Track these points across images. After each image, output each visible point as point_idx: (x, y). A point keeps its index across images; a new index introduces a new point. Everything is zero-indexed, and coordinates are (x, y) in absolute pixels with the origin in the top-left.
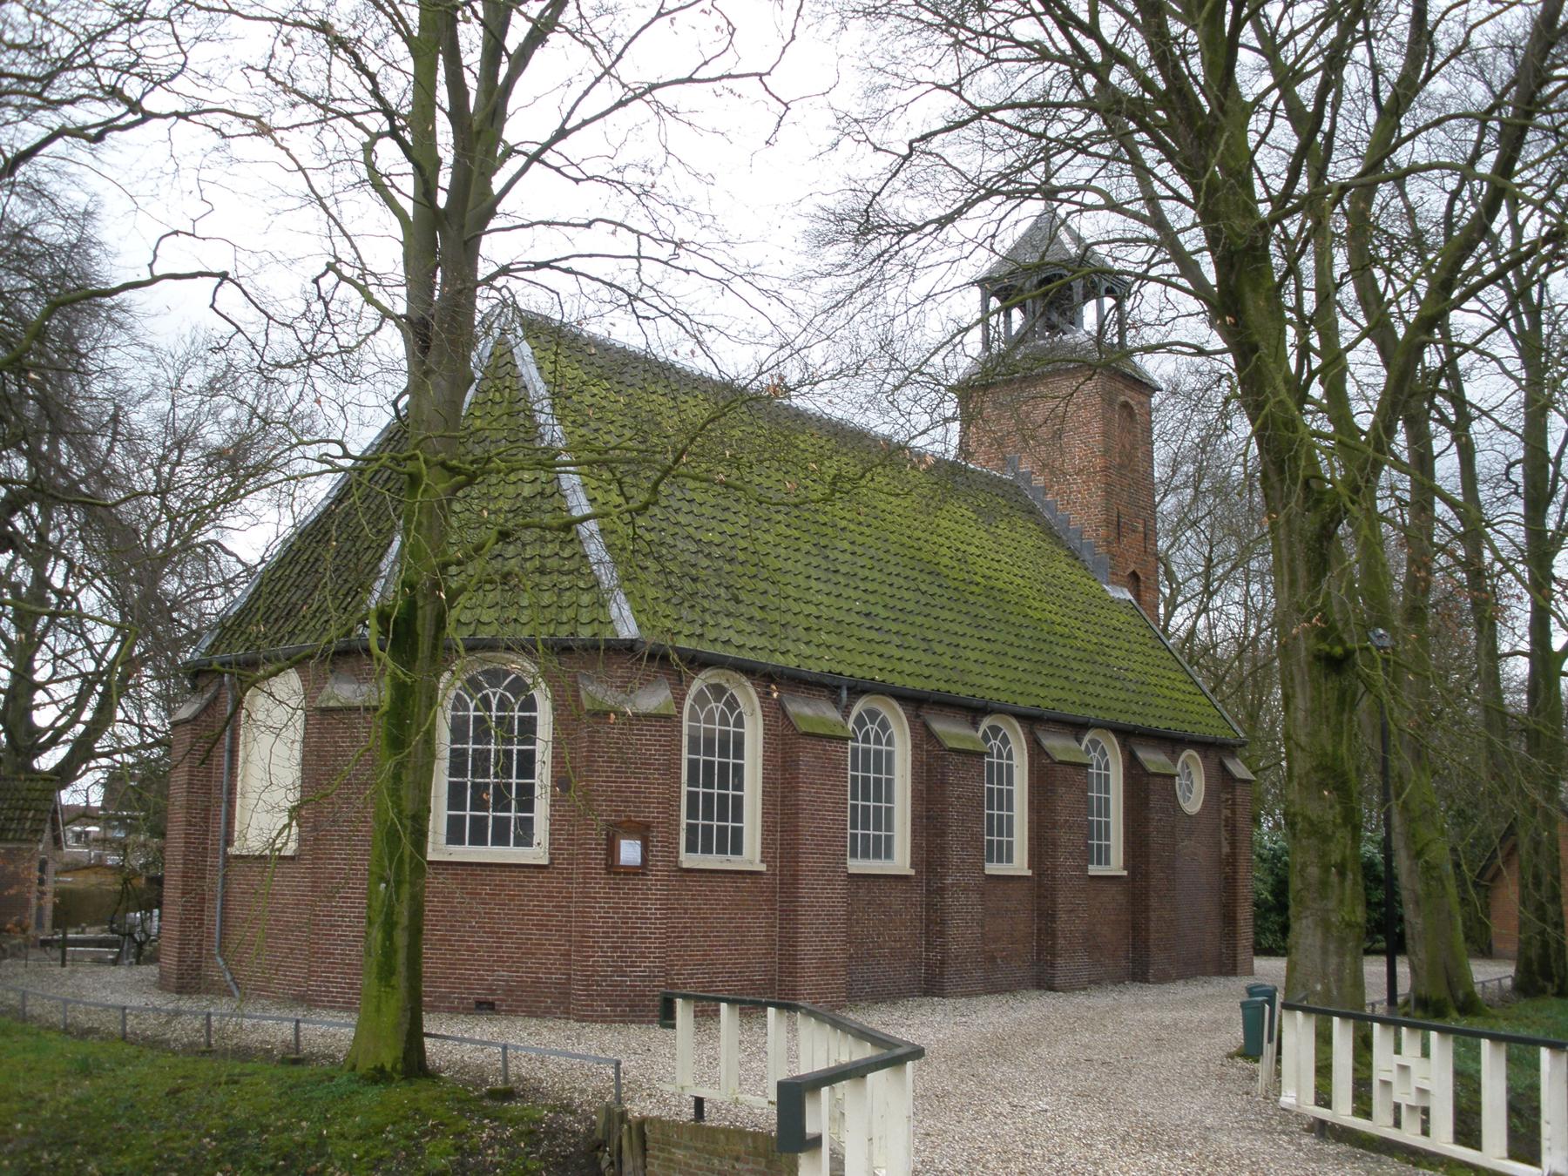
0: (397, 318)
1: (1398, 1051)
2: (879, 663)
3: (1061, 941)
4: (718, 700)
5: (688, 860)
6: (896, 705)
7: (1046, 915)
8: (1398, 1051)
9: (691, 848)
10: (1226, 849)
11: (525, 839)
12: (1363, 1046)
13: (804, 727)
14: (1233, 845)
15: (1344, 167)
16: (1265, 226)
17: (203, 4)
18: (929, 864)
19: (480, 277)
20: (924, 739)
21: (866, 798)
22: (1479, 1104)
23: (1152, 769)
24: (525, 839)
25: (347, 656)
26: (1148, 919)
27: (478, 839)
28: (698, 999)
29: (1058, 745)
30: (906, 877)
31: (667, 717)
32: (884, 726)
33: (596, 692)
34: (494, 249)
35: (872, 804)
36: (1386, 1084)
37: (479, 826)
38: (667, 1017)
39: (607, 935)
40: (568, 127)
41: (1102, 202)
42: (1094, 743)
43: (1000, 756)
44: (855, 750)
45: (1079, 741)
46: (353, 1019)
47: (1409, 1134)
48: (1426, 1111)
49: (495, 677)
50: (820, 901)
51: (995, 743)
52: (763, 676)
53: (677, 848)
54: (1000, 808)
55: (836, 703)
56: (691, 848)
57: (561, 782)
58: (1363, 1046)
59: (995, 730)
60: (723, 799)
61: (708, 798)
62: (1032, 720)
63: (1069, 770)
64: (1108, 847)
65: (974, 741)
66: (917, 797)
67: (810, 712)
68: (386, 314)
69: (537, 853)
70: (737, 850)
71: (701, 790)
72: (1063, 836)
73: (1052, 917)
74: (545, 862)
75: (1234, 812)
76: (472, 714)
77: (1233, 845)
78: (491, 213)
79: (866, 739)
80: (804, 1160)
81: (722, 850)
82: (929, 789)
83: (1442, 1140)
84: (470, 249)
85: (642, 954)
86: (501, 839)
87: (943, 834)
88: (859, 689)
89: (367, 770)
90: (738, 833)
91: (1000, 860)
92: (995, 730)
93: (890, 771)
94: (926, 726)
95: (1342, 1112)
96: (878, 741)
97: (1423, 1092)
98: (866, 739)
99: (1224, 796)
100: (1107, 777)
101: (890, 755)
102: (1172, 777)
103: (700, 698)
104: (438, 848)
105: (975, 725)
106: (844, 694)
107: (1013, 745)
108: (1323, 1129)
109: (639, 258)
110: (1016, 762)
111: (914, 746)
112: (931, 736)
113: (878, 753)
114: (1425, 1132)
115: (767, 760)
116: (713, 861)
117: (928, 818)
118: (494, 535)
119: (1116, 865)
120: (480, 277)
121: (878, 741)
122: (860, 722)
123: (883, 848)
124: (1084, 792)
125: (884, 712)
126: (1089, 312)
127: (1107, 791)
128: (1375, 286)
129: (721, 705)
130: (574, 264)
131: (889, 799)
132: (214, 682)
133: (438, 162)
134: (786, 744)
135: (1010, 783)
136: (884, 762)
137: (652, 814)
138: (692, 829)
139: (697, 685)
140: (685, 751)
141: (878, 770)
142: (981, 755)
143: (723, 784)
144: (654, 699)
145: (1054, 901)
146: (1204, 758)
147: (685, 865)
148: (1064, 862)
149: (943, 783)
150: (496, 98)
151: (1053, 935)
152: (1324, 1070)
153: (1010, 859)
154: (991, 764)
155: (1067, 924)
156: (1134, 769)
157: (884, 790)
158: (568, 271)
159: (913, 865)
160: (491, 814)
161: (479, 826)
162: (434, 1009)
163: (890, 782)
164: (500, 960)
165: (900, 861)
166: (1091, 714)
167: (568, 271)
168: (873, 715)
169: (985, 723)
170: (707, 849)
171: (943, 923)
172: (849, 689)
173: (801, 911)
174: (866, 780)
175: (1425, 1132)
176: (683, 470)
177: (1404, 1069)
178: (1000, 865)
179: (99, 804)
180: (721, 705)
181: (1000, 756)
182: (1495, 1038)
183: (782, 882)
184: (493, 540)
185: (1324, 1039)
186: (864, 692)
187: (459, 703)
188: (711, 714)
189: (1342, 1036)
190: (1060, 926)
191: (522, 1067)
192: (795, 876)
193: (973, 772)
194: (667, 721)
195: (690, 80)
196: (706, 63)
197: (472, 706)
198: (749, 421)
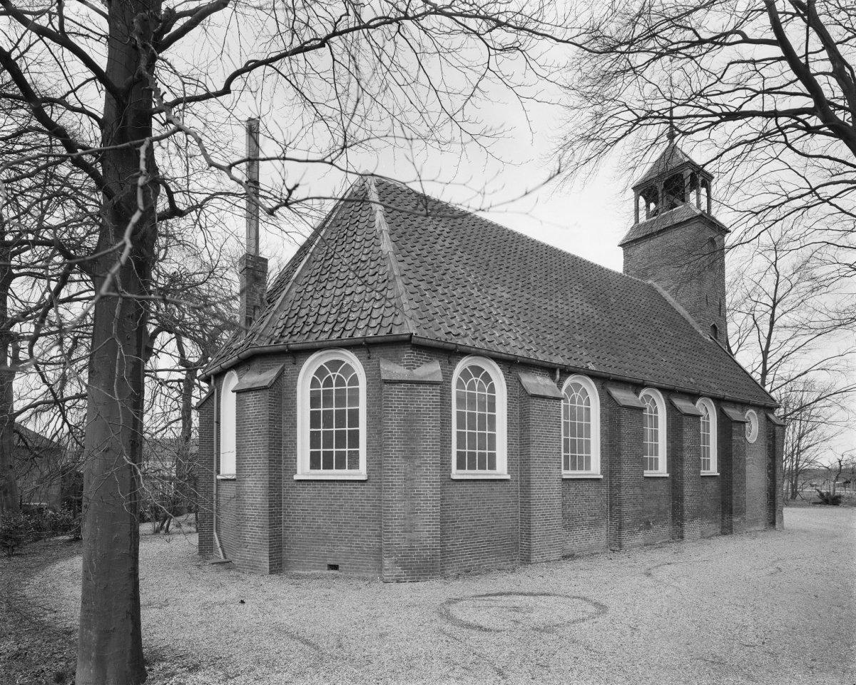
3: (686, 512)
6: (659, 393)
9: (459, 467)
11: (354, 464)
13: (531, 392)
18: (611, 472)
21: (573, 435)
26: (731, 498)
27: (328, 466)
29: (623, 396)
30: (598, 479)
33: (392, 369)
43: (580, 402)
44: (566, 407)
50: (547, 494)
54: (580, 435)
55: (553, 378)
60: (482, 436)
65: (638, 402)
67: (536, 383)
69: (361, 472)
70: (492, 467)
71: (487, 432)
72: (687, 455)
74: (364, 478)
81: (482, 467)
86: (341, 465)
88: (566, 372)
90: (492, 457)
91: (651, 469)
94: (609, 394)
96: (580, 402)
98: (573, 401)
100: (708, 423)
103: (465, 374)
104: (303, 469)
105: (637, 394)
106: (558, 372)
107: (658, 405)
110: (592, 407)
111: (602, 405)
117: (610, 446)
122: (569, 390)
125: (654, 397)
126: (692, 196)
129: (479, 379)
140: (562, 418)
143: (482, 427)
149: (619, 425)
153: (657, 468)
155: (689, 502)
156: (722, 417)
160: (570, 454)
168: (577, 386)
169: (643, 392)
170: (472, 467)
171: (620, 504)
172: (560, 371)
174: (573, 425)
178: (651, 471)
180: (479, 379)
183: (675, 481)
186: (571, 373)
187: (314, 383)
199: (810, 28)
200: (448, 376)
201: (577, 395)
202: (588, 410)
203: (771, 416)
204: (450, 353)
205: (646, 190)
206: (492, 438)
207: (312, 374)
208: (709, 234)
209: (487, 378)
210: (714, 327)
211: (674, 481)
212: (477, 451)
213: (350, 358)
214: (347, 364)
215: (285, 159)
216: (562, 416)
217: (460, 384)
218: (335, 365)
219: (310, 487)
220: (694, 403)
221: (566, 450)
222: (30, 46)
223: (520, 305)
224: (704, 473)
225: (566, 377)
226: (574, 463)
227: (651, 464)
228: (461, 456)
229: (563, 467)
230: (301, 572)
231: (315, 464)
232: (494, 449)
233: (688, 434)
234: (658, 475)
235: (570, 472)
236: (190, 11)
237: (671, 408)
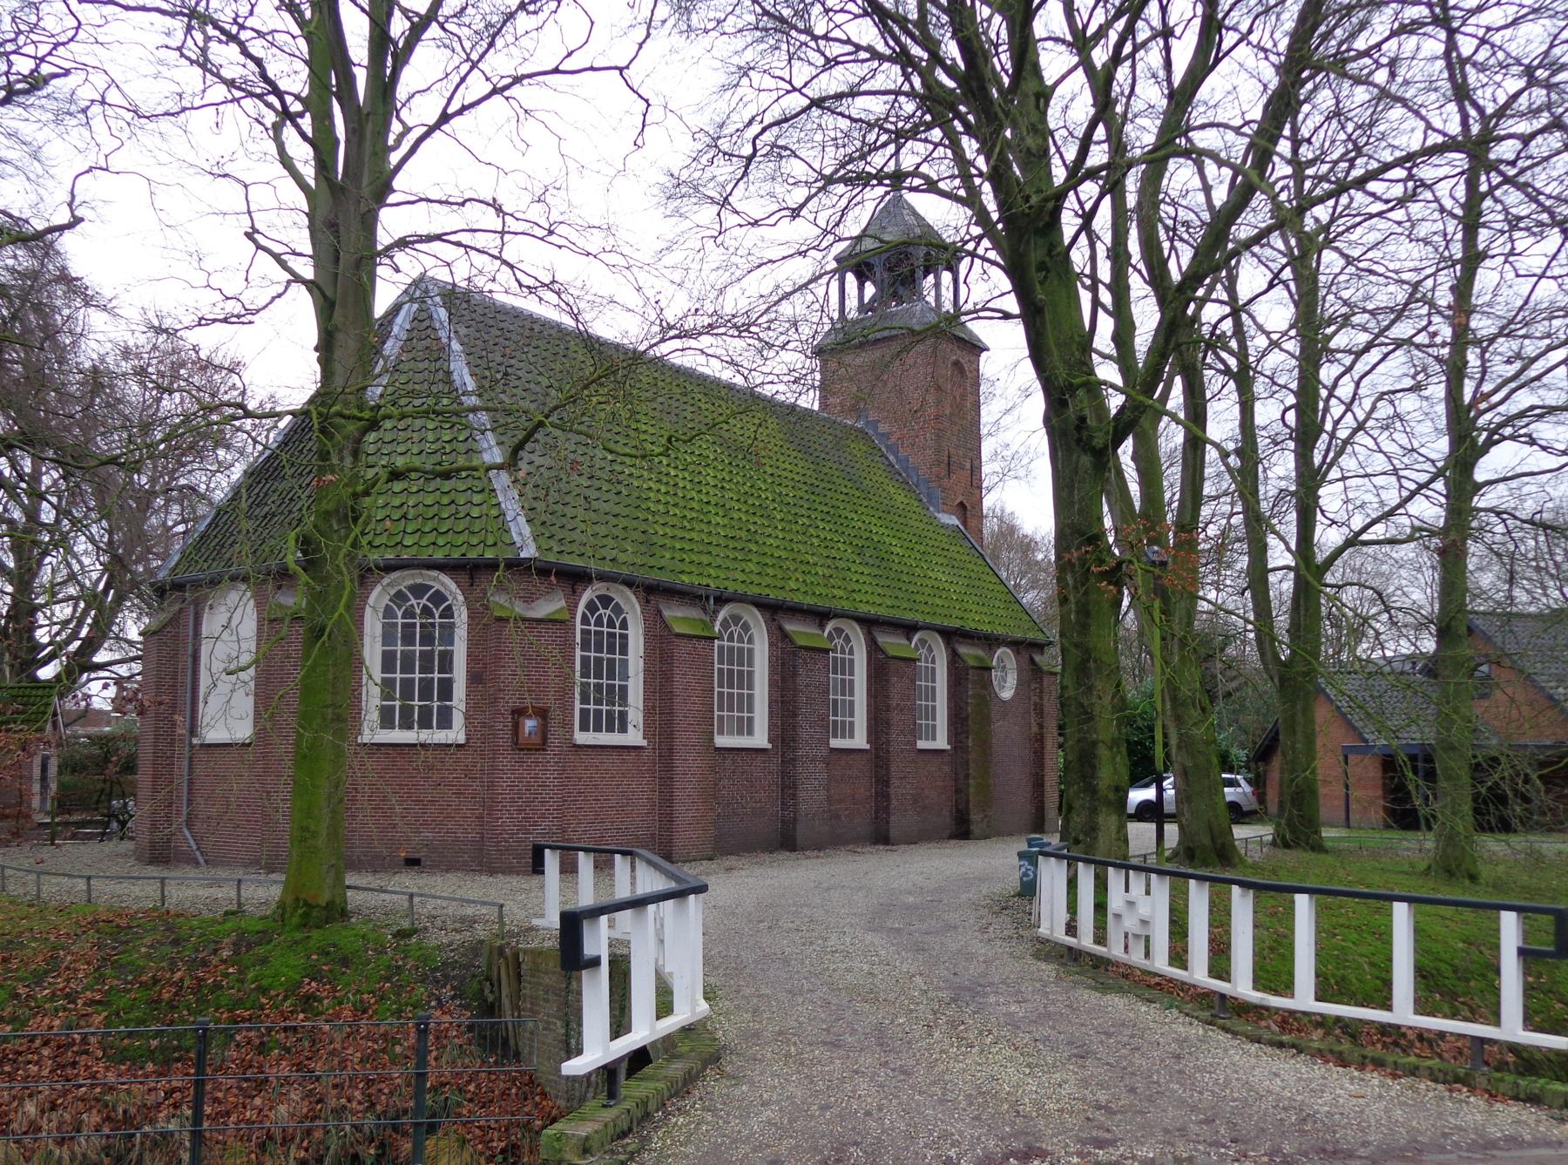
0: (305, 282)
1: (1127, 890)
2: (741, 577)
3: (894, 802)
5: (581, 738)
7: (882, 782)
8: (1127, 890)
10: (1035, 729)
11: (445, 723)
12: (1101, 886)
14: (1041, 726)
15: (1143, 134)
16: (1061, 196)
17: (133, 4)
18: (783, 740)
19: (380, 248)
20: (780, 638)
22: (1498, 930)
24: (445, 723)
25: (283, 576)
28: (594, 851)
29: (892, 643)
31: (562, 622)
32: (746, 627)
34: (392, 223)
35: (604, 708)
36: (1118, 916)
37: (406, 712)
38: (538, 867)
39: (513, 801)
40: (450, 111)
42: (923, 642)
44: (721, 648)
45: (910, 640)
47: (1136, 957)
48: (1147, 939)
49: (419, 590)
51: (839, 642)
53: (572, 728)
54: (741, 687)
56: (584, 727)
57: (474, 678)
58: (1101, 886)
59: (839, 631)
61: (731, 672)
62: (869, 623)
63: (901, 664)
66: (772, 684)
68: (297, 278)
69: (456, 734)
72: (895, 717)
73: (887, 783)
75: (1041, 698)
76: (400, 621)
77: (1041, 726)
78: (387, 188)
79: (731, 639)
80: (585, 974)
81: (610, 729)
82: (783, 678)
83: (1160, 962)
84: (369, 223)
85: (543, 816)
86: (425, 723)
87: (795, 715)
89: (309, 668)
91: (843, 736)
92: (839, 631)
93: (750, 664)
94: (781, 629)
95: (1086, 941)
96: (741, 640)
97: (1144, 923)
98: (731, 639)
99: (1033, 686)
101: (751, 651)
102: (990, 669)
103: (591, 607)
105: (822, 627)
108: (1073, 956)
109: (503, 233)
111: (771, 644)
112: (785, 636)
113: (741, 650)
114: (1147, 955)
116: (605, 738)
118: (384, 475)
120: (380, 248)
121: (741, 640)
123: (746, 727)
124: (913, 681)
125: (746, 617)
127: (934, 681)
128: (1161, 250)
129: (608, 612)
130: (464, 238)
131: (750, 687)
132: (179, 599)
133: (337, 141)
134: (661, 642)
135: (852, 674)
136: (747, 657)
137: (550, 701)
138: (585, 713)
139: (587, 595)
141: (611, 676)
142: (827, 651)
144: (549, 606)
145: (888, 769)
146: (1017, 653)
147: (579, 742)
148: (897, 740)
149: (795, 674)
150: (384, 88)
151: (887, 797)
152: (1072, 907)
154: (835, 659)
155: (900, 789)
157: (746, 680)
158: (458, 244)
159: (770, 741)
161: (406, 712)
162: (1324, 825)
163: (750, 674)
164: (425, 823)
165: (760, 738)
166: (919, 618)
167: (458, 244)
169: (830, 626)
170: (598, 729)
171: (795, 787)
173: (676, 778)
174: (731, 672)
175: (1147, 955)
177: (1131, 904)
181: (843, 652)
182: (1242, 884)
183: (879, 754)
184: (383, 480)
185: (1072, 883)
187: (388, 613)
188: (600, 619)
189: (1086, 877)
190: (892, 791)
191: (426, 908)
192: (671, 750)
193: (819, 665)
194: (560, 624)
195: (556, 71)
196: (569, 54)
197: (400, 614)
198: (606, 377)
199: (1067, 241)
200: (572, 609)
203: (1037, 658)
204: (575, 579)
205: (857, 264)
206: (624, 689)
207: (386, 601)
208: (957, 354)
210: (961, 503)
211: (877, 757)
212: (398, 676)
213: (446, 583)
214: (438, 591)
215: (249, 212)
217: (585, 620)
218: (419, 590)
221: (585, 674)
223: (537, 351)
225: (722, 606)
227: (835, 729)
228: (584, 714)
230: (202, 893)
231: (387, 720)
232: (451, 671)
233: (897, 687)
237: (874, 648)
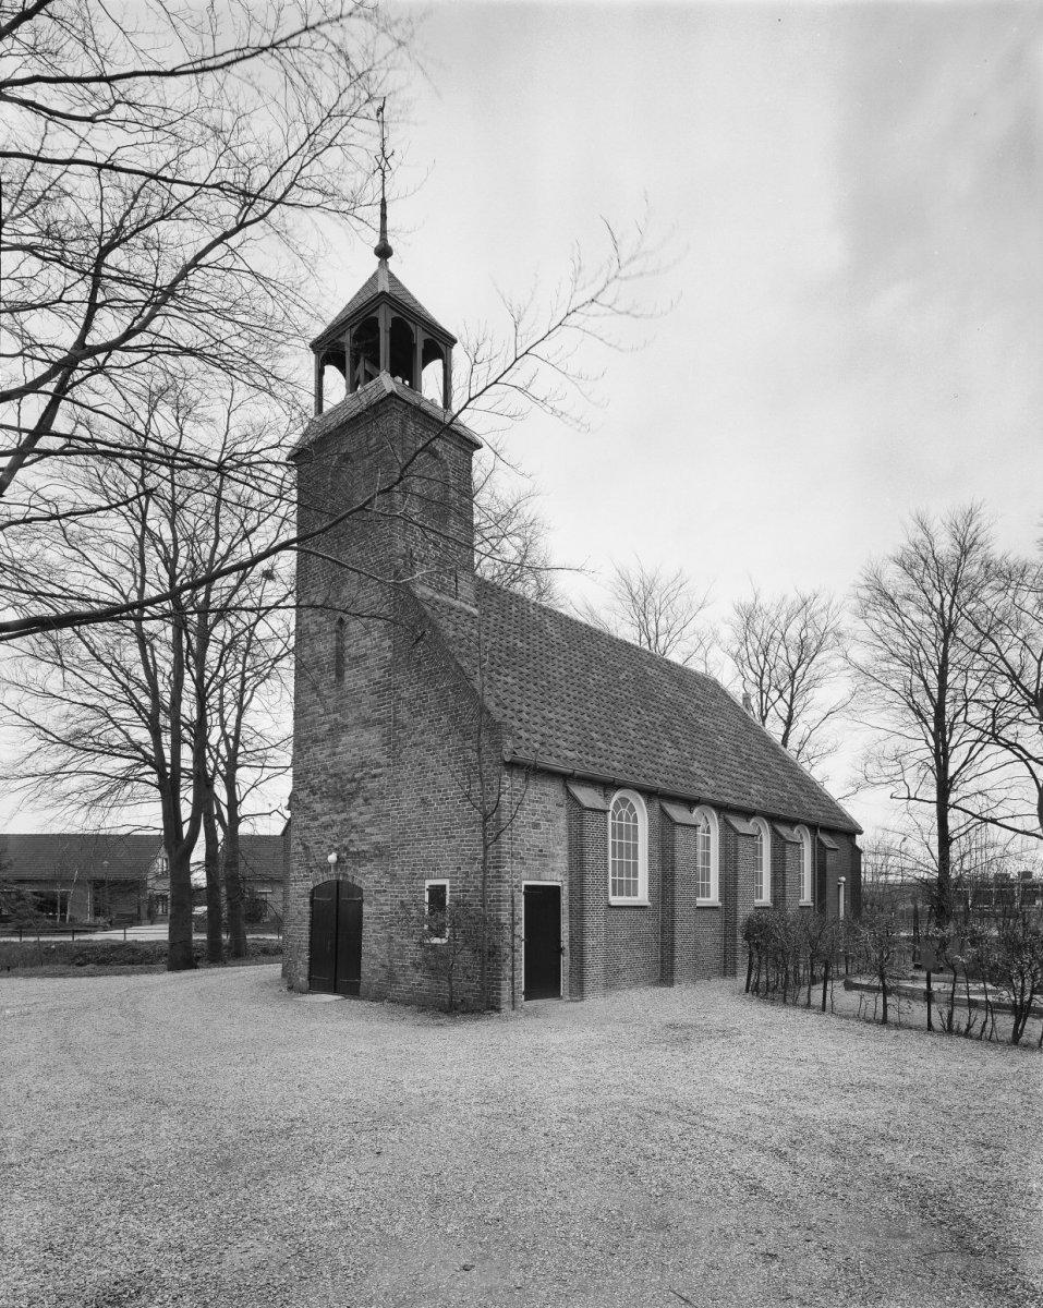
4: (624, 807)
9: (614, 894)
23: (587, 804)
41: (246, 220)
43: (628, 820)
46: (167, 926)
52: (650, 794)
56: (614, 894)
64: (708, 885)
81: (629, 895)
91: (703, 896)
92: (624, 801)
98: (620, 819)
107: (638, 812)
110: (639, 824)
115: (813, 888)
119: (714, 898)
121: (628, 820)
153: (708, 896)
168: (624, 801)
176: (119, 499)
178: (629, 898)
179: (274, 827)
195: (517, 359)
201: (624, 810)
202: (636, 828)
209: (632, 809)
216: (610, 834)
219: (707, 912)
220: (691, 812)
222: (994, 821)
224: (701, 901)
226: (619, 889)
227: (628, 888)
229: (448, 889)
234: (637, 904)
235: (620, 898)
236: (123, 335)
